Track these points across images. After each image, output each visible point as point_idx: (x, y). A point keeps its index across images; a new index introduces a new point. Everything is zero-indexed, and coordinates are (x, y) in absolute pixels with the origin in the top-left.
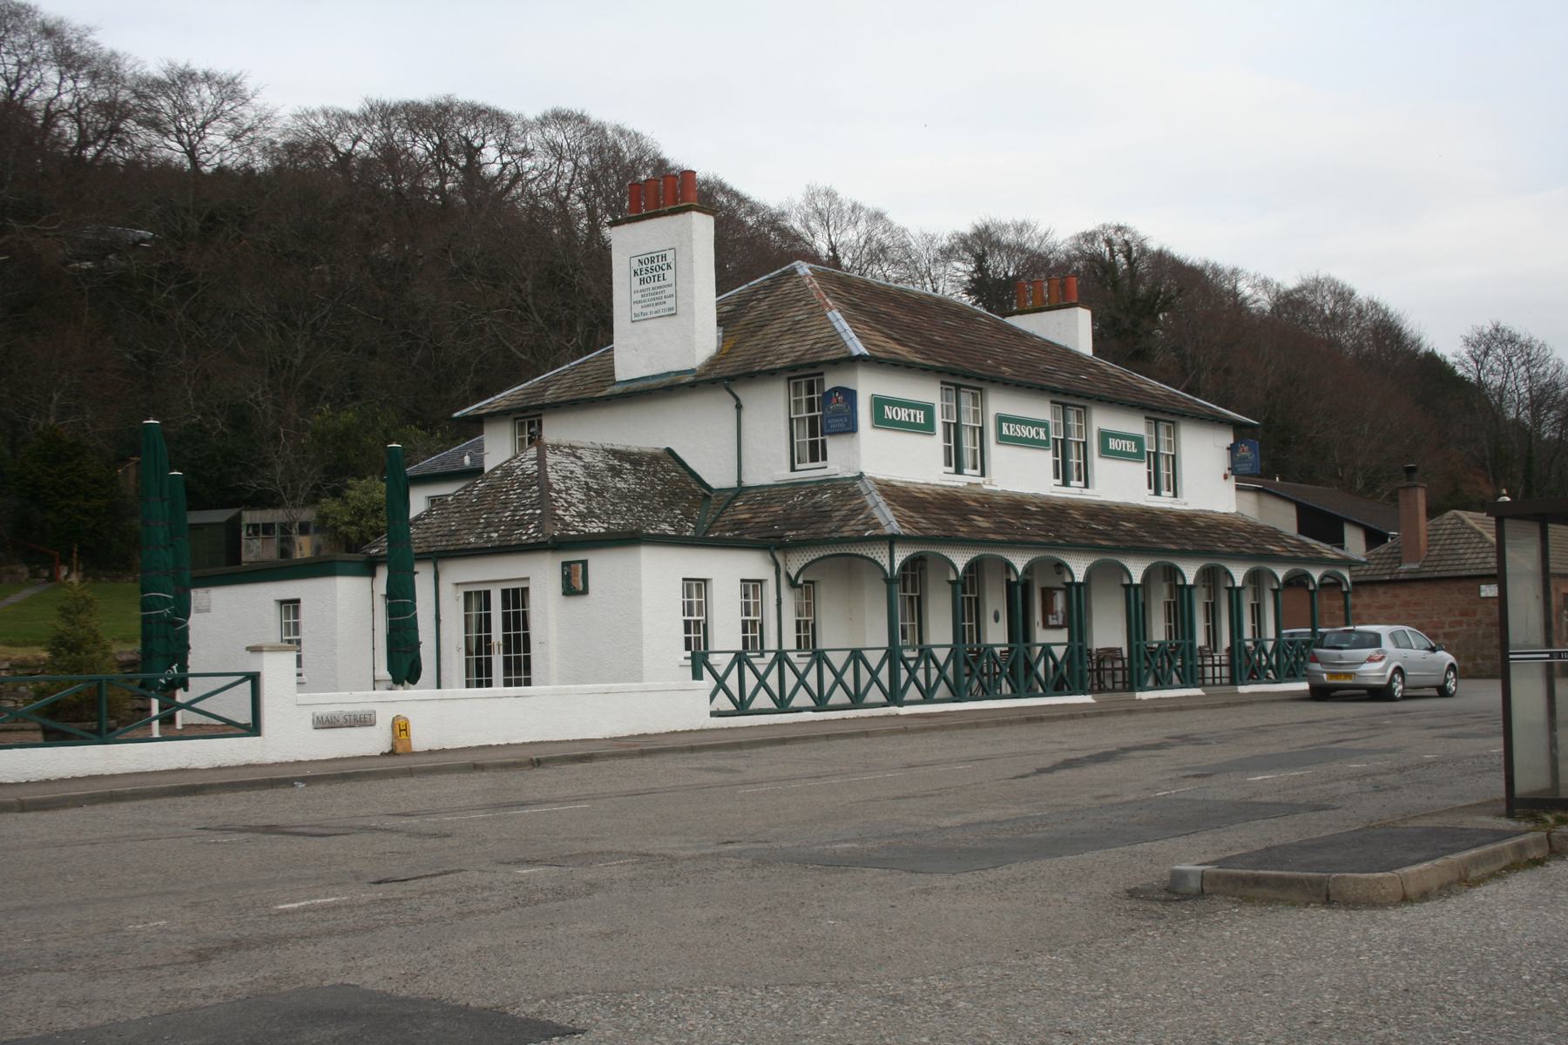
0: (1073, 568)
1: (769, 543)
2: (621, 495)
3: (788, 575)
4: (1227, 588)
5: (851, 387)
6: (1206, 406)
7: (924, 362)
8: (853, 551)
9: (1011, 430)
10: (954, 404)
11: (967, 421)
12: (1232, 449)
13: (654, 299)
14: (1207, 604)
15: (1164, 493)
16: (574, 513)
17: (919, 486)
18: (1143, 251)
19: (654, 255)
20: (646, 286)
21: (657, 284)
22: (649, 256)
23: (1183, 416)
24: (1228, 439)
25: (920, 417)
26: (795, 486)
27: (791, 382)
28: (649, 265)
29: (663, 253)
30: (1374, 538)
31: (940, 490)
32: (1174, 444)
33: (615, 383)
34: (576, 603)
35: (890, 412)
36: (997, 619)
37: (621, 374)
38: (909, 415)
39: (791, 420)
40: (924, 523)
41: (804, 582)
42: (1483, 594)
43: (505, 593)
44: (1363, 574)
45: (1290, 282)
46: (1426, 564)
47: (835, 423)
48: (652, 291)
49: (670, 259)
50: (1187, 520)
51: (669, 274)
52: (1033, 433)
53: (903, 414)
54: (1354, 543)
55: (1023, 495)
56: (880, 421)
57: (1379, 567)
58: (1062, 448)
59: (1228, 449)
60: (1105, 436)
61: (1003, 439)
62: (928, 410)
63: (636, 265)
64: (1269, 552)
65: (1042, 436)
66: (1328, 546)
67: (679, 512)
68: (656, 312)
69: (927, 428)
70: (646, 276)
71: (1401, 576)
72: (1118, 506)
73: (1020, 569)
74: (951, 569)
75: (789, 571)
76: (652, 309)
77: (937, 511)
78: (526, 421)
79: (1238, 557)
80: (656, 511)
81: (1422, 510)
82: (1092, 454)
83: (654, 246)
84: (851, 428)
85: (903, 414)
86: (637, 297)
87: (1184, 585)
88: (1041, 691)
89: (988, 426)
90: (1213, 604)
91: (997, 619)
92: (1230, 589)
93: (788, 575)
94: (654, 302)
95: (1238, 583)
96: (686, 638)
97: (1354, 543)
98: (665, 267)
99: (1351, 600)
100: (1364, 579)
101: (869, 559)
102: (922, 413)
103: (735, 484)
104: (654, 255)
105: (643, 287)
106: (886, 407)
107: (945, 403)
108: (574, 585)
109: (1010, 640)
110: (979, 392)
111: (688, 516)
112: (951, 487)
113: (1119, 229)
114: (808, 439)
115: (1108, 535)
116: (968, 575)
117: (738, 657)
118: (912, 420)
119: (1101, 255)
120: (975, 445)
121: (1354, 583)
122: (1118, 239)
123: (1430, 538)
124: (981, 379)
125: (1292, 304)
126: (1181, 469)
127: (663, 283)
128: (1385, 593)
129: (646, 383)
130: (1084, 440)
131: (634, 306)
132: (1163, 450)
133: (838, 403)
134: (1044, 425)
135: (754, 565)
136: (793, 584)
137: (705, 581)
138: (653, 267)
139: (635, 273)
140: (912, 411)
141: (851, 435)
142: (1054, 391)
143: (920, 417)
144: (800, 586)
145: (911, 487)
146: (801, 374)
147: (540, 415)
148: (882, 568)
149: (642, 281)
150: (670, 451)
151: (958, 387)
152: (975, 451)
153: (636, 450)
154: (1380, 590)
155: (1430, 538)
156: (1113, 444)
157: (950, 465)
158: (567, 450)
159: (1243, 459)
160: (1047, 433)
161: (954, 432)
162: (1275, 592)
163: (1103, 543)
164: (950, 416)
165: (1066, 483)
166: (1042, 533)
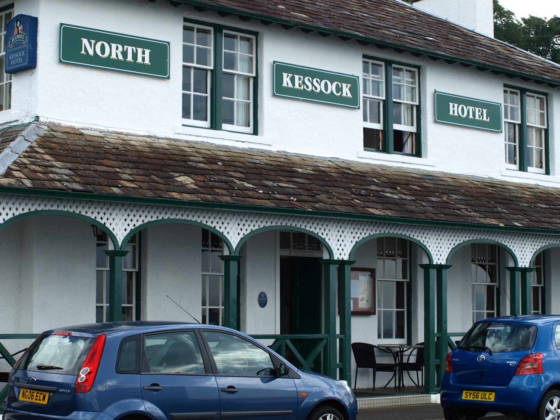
0: (518, 256)
4: (422, 266)
5: (33, 15)
7: (240, 9)
9: (297, 82)
10: (519, 107)
23: (267, 22)
36: (263, 302)
38: (125, 54)
72: (454, 178)
82: (426, 118)
89: (425, 105)
90: (543, 289)
91: (263, 302)
124: (417, 54)
126: (553, 145)
134: (352, 81)
140: (130, 49)
151: (523, 91)
156: (454, 109)
157: (541, 167)
160: (354, 90)
164: (368, 92)
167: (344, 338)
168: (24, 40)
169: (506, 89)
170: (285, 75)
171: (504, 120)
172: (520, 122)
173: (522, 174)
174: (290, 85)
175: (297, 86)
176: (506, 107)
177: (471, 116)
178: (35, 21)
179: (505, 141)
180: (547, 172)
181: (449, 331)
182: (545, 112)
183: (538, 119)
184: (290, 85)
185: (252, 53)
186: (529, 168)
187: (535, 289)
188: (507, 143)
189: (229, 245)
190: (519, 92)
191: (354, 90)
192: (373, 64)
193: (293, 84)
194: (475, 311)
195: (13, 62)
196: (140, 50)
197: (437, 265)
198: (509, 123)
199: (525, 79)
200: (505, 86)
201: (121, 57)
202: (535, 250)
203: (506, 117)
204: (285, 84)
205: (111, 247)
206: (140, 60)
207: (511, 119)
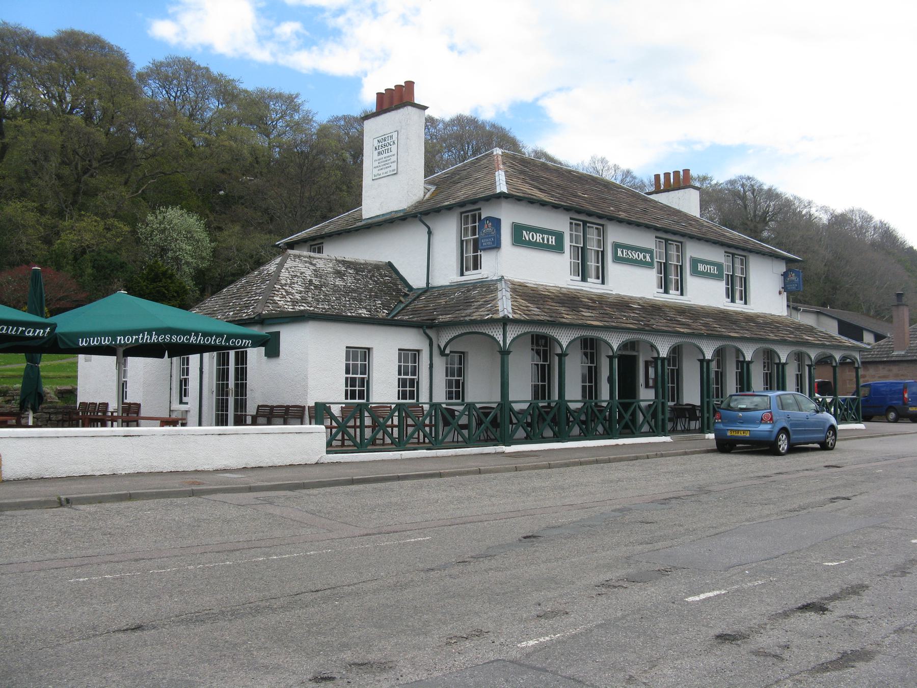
1: (426, 326)
2: (336, 289)
3: (439, 347)
4: (557, 355)
6: (767, 247)
8: (480, 331)
11: (592, 246)
12: (785, 275)
13: (385, 165)
14: (797, 375)
15: (738, 301)
16: (289, 300)
17: (547, 288)
18: (761, 190)
19: (386, 136)
20: (381, 156)
21: (387, 155)
22: (383, 137)
23: (611, 219)
24: (782, 268)
25: (552, 240)
26: (459, 286)
27: (463, 215)
28: (383, 143)
29: (391, 134)
30: (878, 337)
31: (564, 291)
32: (745, 270)
33: (361, 220)
34: (274, 362)
35: (526, 235)
37: (366, 215)
38: (543, 239)
39: (462, 242)
40: (535, 310)
41: (451, 352)
42: (697, 402)
43: (237, 353)
44: (869, 357)
45: (839, 210)
46: (909, 351)
47: (485, 242)
48: (384, 160)
49: (395, 138)
50: (750, 319)
51: (394, 148)
52: (641, 256)
53: (538, 238)
54: (868, 338)
55: (631, 298)
56: (518, 240)
57: (880, 353)
58: (664, 269)
59: (782, 275)
60: (695, 262)
61: (617, 259)
62: (559, 236)
63: (376, 144)
64: (805, 341)
65: (648, 259)
66: (846, 339)
67: (380, 302)
68: (386, 173)
69: (558, 248)
70: (381, 150)
71: (893, 359)
72: (702, 307)
73: (615, 347)
74: (556, 343)
75: (440, 344)
76: (384, 171)
77: (554, 304)
78: (317, 247)
79: (783, 342)
80: (360, 301)
81: (907, 320)
82: (686, 273)
83: (387, 130)
84: (496, 245)
85: (538, 238)
86: (376, 164)
87: (744, 361)
88: (600, 429)
90: (801, 375)
92: (778, 364)
93: (439, 347)
94: (385, 167)
95: (748, 358)
96: (583, 386)
97: (868, 338)
98: (392, 143)
99: (861, 372)
100: (871, 360)
101: (489, 336)
102: (554, 237)
103: (425, 285)
104: (386, 136)
105: (380, 157)
106: (524, 232)
107: (574, 233)
108: (272, 347)
109: (584, 396)
110: (601, 228)
111: (384, 306)
112: (575, 289)
113: (749, 178)
114: (472, 254)
115: (689, 325)
116: (672, 355)
117: (398, 407)
118: (546, 242)
119: (739, 191)
120: (598, 263)
121: (863, 363)
122: (748, 183)
123: (911, 336)
124: (600, 217)
125: (840, 221)
127: (390, 154)
128: (884, 368)
129: (384, 218)
130: (681, 264)
131: (374, 170)
132: (738, 274)
133: (488, 228)
134: (650, 252)
135: (411, 340)
136: (442, 353)
137: (369, 349)
138: (384, 144)
139: (376, 148)
141: (496, 250)
142: (657, 229)
143: (552, 240)
144: (447, 355)
145: (541, 288)
146: (468, 209)
147: (322, 243)
148: (498, 342)
149: (379, 154)
150: (390, 264)
152: (598, 267)
153: (363, 262)
154: (881, 367)
155: (911, 336)
156: (701, 267)
158: (306, 259)
159: (792, 282)
160: (652, 257)
161: (581, 254)
162: (810, 366)
163: (682, 330)
165: (666, 292)
166: (635, 322)
167: (341, 405)
168: (493, 231)
169: (572, 221)
170: (619, 249)
171: (655, 260)
172: (664, 261)
173: (681, 297)
174: (621, 256)
175: (624, 256)
176: (656, 251)
177: (709, 271)
178: (499, 221)
179: (571, 259)
180: (682, 294)
181: (510, 399)
182: (602, 238)
183: (595, 243)
184: (621, 256)
185: (600, 237)
186: (589, 280)
187: (717, 372)
188: (572, 260)
189: (836, 361)
190: (731, 255)
191: (652, 257)
192: (575, 224)
193: (623, 255)
194: (244, 382)
195: (484, 244)
196: (550, 237)
197: (662, 358)
198: (574, 246)
199: (737, 248)
200: (571, 219)
201: (541, 241)
202: (569, 340)
203: (656, 258)
204: (619, 255)
205: (834, 364)
206: (550, 243)
207: (660, 259)
